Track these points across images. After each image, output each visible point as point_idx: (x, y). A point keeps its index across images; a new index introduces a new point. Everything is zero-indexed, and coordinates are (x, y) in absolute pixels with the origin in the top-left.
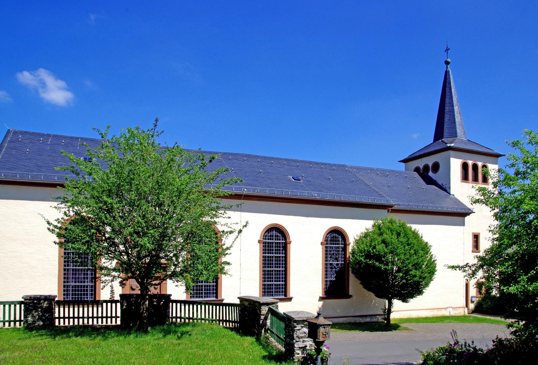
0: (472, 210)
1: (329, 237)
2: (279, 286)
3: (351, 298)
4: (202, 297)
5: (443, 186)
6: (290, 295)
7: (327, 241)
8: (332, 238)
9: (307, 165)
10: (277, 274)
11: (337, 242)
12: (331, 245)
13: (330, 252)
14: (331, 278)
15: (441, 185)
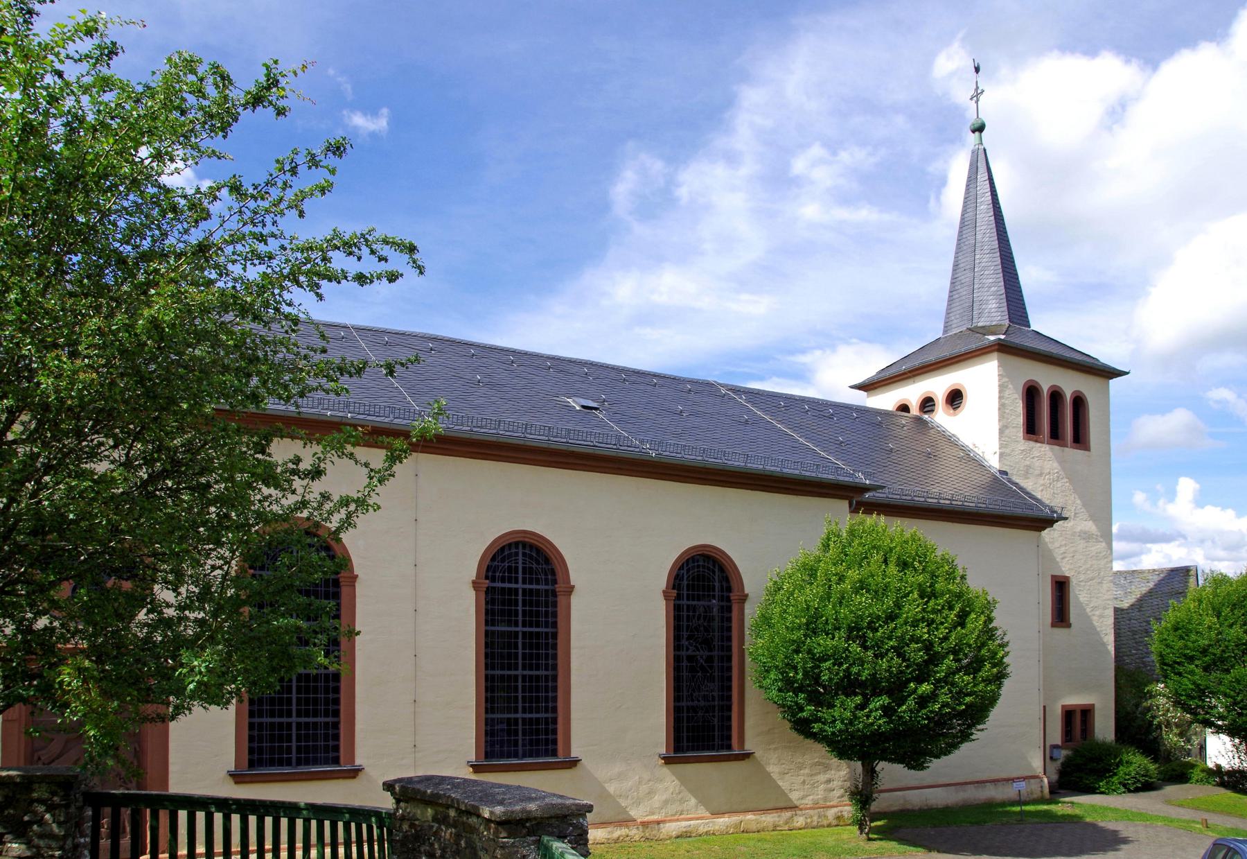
0: (1059, 511)
2: (538, 724)
3: (575, 765)
4: (289, 763)
5: (976, 450)
6: (164, 780)
8: (693, 579)
9: (613, 374)
10: (531, 687)
12: (691, 603)
13: (688, 621)
14: (693, 701)
15: (971, 447)
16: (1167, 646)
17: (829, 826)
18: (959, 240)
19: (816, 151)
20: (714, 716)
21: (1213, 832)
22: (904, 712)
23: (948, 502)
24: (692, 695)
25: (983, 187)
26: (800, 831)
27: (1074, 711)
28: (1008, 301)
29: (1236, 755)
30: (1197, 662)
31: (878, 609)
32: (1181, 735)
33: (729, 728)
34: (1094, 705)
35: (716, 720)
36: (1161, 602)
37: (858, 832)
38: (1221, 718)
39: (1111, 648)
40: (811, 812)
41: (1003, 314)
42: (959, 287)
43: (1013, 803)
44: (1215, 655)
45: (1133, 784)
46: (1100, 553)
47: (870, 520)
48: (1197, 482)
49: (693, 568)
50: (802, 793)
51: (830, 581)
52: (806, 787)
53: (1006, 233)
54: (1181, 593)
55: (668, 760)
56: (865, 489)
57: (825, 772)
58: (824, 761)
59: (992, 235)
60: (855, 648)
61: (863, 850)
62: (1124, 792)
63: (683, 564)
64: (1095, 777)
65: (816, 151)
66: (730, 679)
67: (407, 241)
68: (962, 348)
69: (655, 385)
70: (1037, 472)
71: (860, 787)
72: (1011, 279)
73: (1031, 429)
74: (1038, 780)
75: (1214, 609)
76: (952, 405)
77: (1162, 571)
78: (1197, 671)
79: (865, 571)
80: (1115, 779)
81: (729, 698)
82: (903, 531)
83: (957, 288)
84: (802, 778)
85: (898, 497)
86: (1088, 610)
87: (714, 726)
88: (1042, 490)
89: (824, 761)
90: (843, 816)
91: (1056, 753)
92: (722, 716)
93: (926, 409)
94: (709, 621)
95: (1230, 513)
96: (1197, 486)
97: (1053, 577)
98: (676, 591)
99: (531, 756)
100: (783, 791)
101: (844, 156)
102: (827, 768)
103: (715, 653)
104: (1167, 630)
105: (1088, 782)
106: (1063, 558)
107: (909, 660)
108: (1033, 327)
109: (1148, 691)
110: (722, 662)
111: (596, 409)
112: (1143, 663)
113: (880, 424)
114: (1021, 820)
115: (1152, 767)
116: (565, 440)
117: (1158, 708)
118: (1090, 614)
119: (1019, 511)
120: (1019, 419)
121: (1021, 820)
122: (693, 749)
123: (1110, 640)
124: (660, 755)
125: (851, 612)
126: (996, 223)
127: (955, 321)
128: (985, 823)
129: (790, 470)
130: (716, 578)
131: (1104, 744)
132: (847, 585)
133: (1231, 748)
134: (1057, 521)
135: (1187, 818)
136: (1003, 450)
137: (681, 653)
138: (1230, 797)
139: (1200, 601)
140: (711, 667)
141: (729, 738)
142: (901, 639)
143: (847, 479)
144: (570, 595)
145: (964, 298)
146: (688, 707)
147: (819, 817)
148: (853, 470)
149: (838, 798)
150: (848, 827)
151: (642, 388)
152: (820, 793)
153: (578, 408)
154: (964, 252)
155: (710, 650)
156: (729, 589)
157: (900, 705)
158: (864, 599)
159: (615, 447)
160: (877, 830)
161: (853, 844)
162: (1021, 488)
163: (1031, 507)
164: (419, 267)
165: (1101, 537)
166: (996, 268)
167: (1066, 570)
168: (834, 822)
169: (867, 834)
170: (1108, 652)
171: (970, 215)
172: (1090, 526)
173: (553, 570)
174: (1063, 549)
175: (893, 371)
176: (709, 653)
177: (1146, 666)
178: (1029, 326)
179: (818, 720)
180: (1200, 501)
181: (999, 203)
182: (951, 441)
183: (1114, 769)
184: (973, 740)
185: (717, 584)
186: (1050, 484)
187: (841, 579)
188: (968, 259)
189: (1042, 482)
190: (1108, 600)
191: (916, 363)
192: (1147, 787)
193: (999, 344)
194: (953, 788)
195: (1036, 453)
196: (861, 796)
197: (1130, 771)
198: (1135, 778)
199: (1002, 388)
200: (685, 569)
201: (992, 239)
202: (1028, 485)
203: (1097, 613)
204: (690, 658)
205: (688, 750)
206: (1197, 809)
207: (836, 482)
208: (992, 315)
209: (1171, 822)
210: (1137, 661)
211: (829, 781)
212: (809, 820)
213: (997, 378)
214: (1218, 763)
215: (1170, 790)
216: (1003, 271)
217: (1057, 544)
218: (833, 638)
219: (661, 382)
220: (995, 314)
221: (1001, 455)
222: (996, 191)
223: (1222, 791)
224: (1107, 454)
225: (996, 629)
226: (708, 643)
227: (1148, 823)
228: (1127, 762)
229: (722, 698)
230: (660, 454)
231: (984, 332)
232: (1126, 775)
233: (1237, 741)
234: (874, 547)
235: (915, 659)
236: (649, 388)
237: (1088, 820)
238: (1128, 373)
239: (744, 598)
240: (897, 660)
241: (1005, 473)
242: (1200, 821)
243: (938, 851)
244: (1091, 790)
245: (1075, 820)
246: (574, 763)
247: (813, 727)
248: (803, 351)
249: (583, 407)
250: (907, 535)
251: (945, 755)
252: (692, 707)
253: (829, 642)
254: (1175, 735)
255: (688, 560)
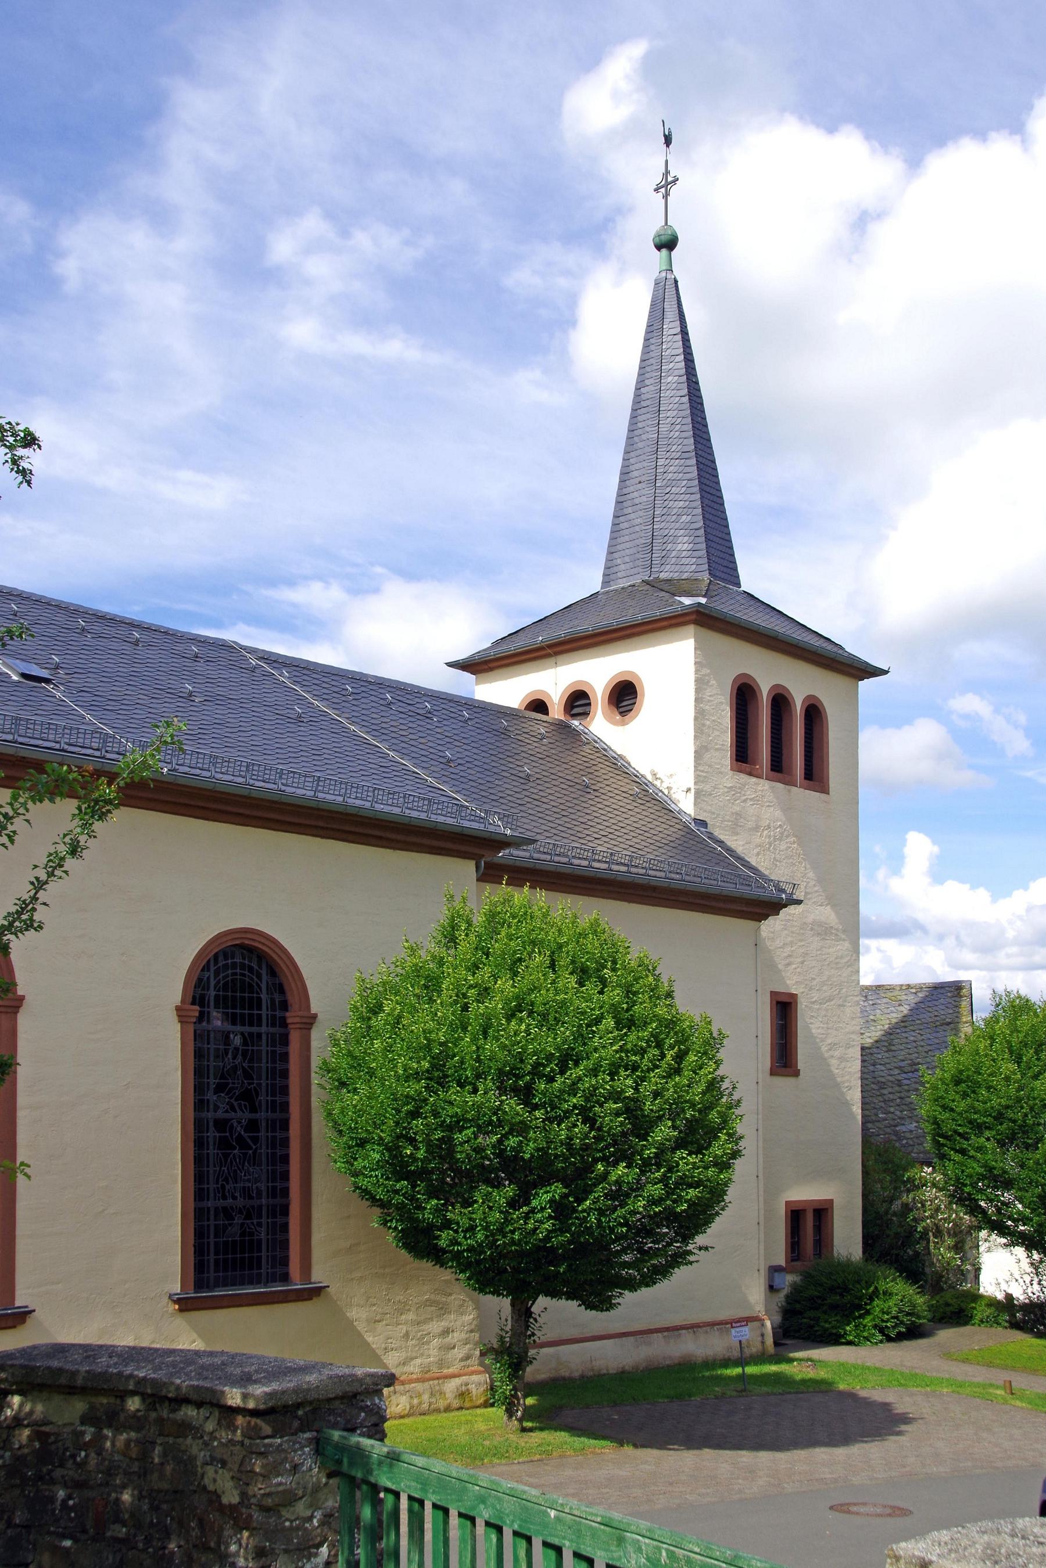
1: (213, 983)
5: (657, 783)
7: (201, 1005)
9: (61, 618)
11: (251, 1008)
14: (225, 1198)
15: (650, 777)
16: (944, 1107)
17: (448, 1409)
18: (630, 431)
19: (313, 223)
20: (260, 1225)
21: (1022, 1401)
22: (588, 1211)
23: (624, 869)
24: (223, 1186)
25: (673, 346)
26: (402, 1421)
27: (804, 1210)
28: (707, 540)
29: (1036, 1280)
30: (987, 1134)
31: (549, 1043)
32: (958, 1248)
33: (285, 1245)
34: (831, 1201)
35: (263, 1229)
36: (920, 1038)
37: (505, 1418)
38: (1025, 1220)
39: (857, 1110)
40: (419, 1386)
41: (700, 561)
42: (630, 510)
43: (727, 1363)
44: (1014, 1121)
45: (894, 1327)
46: (842, 957)
47: (521, 896)
48: (934, 842)
49: (226, 967)
50: (404, 1355)
51: (465, 996)
52: (410, 1343)
53: (706, 426)
54: (948, 1024)
55: (185, 1304)
56: (501, 843)
57: (440, 1317)
58: (438, 1298)
59: (685, 428)
60: (512, 1106)
61: (517, 1448)
62: (881, 1342)
63: (209, 961)
64: (838, 1318)
65: (313, 223)
66: (285, 1159)
67: (21, 427)
68: (635, 613)
69: (136, 643)
70: (751, 824)
71: (508, 1339)
72: (712, 504)
73: (742, 755)
74: (756, 1324)
75: (1011, 1052)
76: (618, 707)
77: (920, 988)
78: (988, 1145)
79: (523, 983)
80: (867, 1321)
81: (286, 1192)
82: (576, 917)
83: (626, 511)
84: (404, 1329)
85: (548, 857)
86: (824, 1049)
87: (260, 1241)
88: (758, 854)
89: (438, 1298)
90: (469, 1392)
91: (778, 1278)
92: (274, 1223)
93: (576, 711)
94: (251, 1060)
95: (983, 894)
96: (936, 849)
97: (773, 994)
98: (197, 1008)
99: (225, 1285)
100: (373, 1350)
101: (362, 239)
102: (443, 1310)
103: (262, 1115)
104: (943, 1083)
105: (827, 1325)
106: (788, 964)
107: (600, 1129)
108: (743, 588)
109: (909, 1178)
110: (274, 1130)
111: (47, 681)
112: (896, 1133)
113: (505, 733)
114: (745, 1390)
115: (920, 1300)
116: (10, 737)
117: (923, 1206)
118: (826, 1055)
119: (730, 888)
120: (726, 738)
121: (745, 1390)
122: (227, 1283)
123: (855, 1096)
124: (170, 1296)
125: (503, 1047)
126: (692, 407)
127: (623, 567)
128: (690, 1396)
129: (387, 807)
130: (264, 986)
131: (849, 1263)
132: (496, 1004)
133: (1029, 1270)
134: (785, 906)
135: (979, 1379)
136: (701, 786)
137: (204, 1115)
138: (1031, 1346)
139: (992, 1038)
140: (255, 1140)
141: (285, 1261)
142: (590, 1095)
143: (475, 825)
144: (16, 1013)
145: (637, 528)
146: (216, 1209)
147: (432, 1395)
148: (486, 812)
149: (462, 1360)
150: (479, 1411)
151: (115, 645)
152: (432, 1353)
153: (15, 678)
154: (639, 452)
155: (254, 1109)
156: (285, 1006)
157: (580, 1201)
158: (523, 1027)
159: (98, 754)
160: (529, 1414)
161: (498, 1439)
162: (729, 850)
163: (746, 881)
164: (23, 472)
165: (844, 931)
166: (690, 484)
167: (792, 984)
168: (456, 1403)
169: (520, 1420)
170: (853, 1115)
171: (649, 391)
172: (826, 914)
173: (281, 985)
174: (788, 950)
175: (520, 644)
176: (253, 1116)
177: (900, 1139)
178: (739, 585)
179: (447, 1224)
180: (938, 874)
181: (696, 376)
182: (618, 765)
183: (866, 1304)
184: (691, 1263)
185: (264, 996)
186: (770, 844)
187: (485, 992)
188: (645, 464)
189: (758, 841)
190: (853, 1033)
191: (561, 632)
192: (913, 1332)
193: (698, 612)
194: (631, 1339)
195: (750, 794)
196: (510, 1355)
197: (890, 1307)
198: (896, 1318)
199: (700, 684)
200: (212, 969)
201: (684, 435)
202: (737, 843)
203: (837, 1053)
204: (221, 1125)
205: (217, 1285)
206: (989, 1365)
207: (459, 830)
208: (684, 561)
209: (961, 1387)
210: (888, 1130)
211: (446, 1332)
212: (415, 1401)
213: (692, 668)
214: (1010, 1291)
215: (946, 1335)
216: (701, 490)
217: (778, 943)
218: (475, 1091)
219: (145, 637)
220: (687, 561)
221: (698, 794)
222: (691, 354)
223: (1019, 1336)
224: (854, 801)
225: (722, 1079)
226: (248, 1097)
227: (928, 1389)
228: (885, 1293)
229: (273, 1193)
230: (175, 770)
231: (673, 589)
232: (884, 1313)
233: (1036, 1256)
234: (533, 943)
235: (611, 1128)
236: (128, 648)
237: (842, 1387)
238: (885, 672)
239: (311, 1020)
240: (581, 1128)
241: (703, 823)
242: (1001, 1383)
243: (636, 1446)
244: (834, 1339)
245: (823, 1387)
246: (316, 1292)
247: (438, 1237)
248: (291, 582)
249: (24, 676)
250: (584, 923)
251: (647, 1285)
252: (225, 1209)
253: (470, 1099)
254: (949, 1248)
255: (216, 956)
